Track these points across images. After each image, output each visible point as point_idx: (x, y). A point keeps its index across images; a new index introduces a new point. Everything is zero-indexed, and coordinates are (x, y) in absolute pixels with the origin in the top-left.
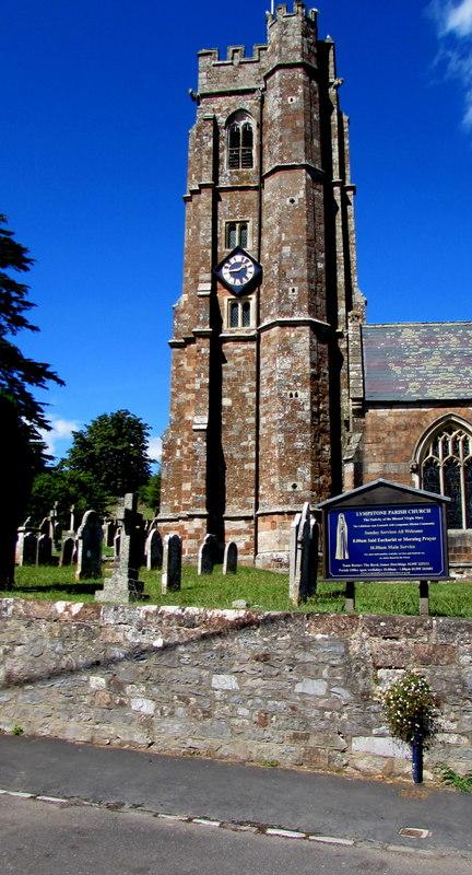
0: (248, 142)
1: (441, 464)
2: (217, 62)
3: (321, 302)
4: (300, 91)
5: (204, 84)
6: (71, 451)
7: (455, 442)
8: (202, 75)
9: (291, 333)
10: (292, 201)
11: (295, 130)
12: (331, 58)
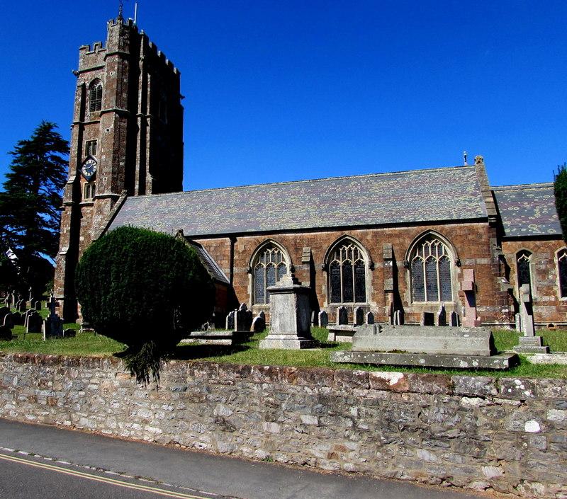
0: (100, 96)
1: (341, 264)
2: (88, 52)
4: (116, 68)
5: (81, 67)
7: (433, 246)
8: (81, 60)
9: (102, 202)
10: (108, 130)
11: (112, 91)
12: (142, 43)
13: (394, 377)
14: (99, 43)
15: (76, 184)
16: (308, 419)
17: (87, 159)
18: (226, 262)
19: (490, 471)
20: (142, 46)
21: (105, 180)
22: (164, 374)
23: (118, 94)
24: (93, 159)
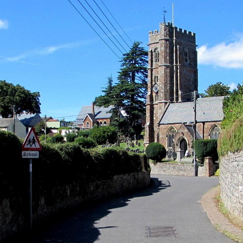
3: (168, 96)
4: (164, 46)
6: (212, 85)
9: (161, 105)
11: (163, 56)
13: (179, 164)
14: (157, 31)
15: (151, 96)
16: (172, 169)
17: (155, 84)
18: (202, 132)
19: (186, 173)
20: (174, 33)
21: (161, 95)
22: (158, 164)
23: (165, 58)
24: (157, 84)
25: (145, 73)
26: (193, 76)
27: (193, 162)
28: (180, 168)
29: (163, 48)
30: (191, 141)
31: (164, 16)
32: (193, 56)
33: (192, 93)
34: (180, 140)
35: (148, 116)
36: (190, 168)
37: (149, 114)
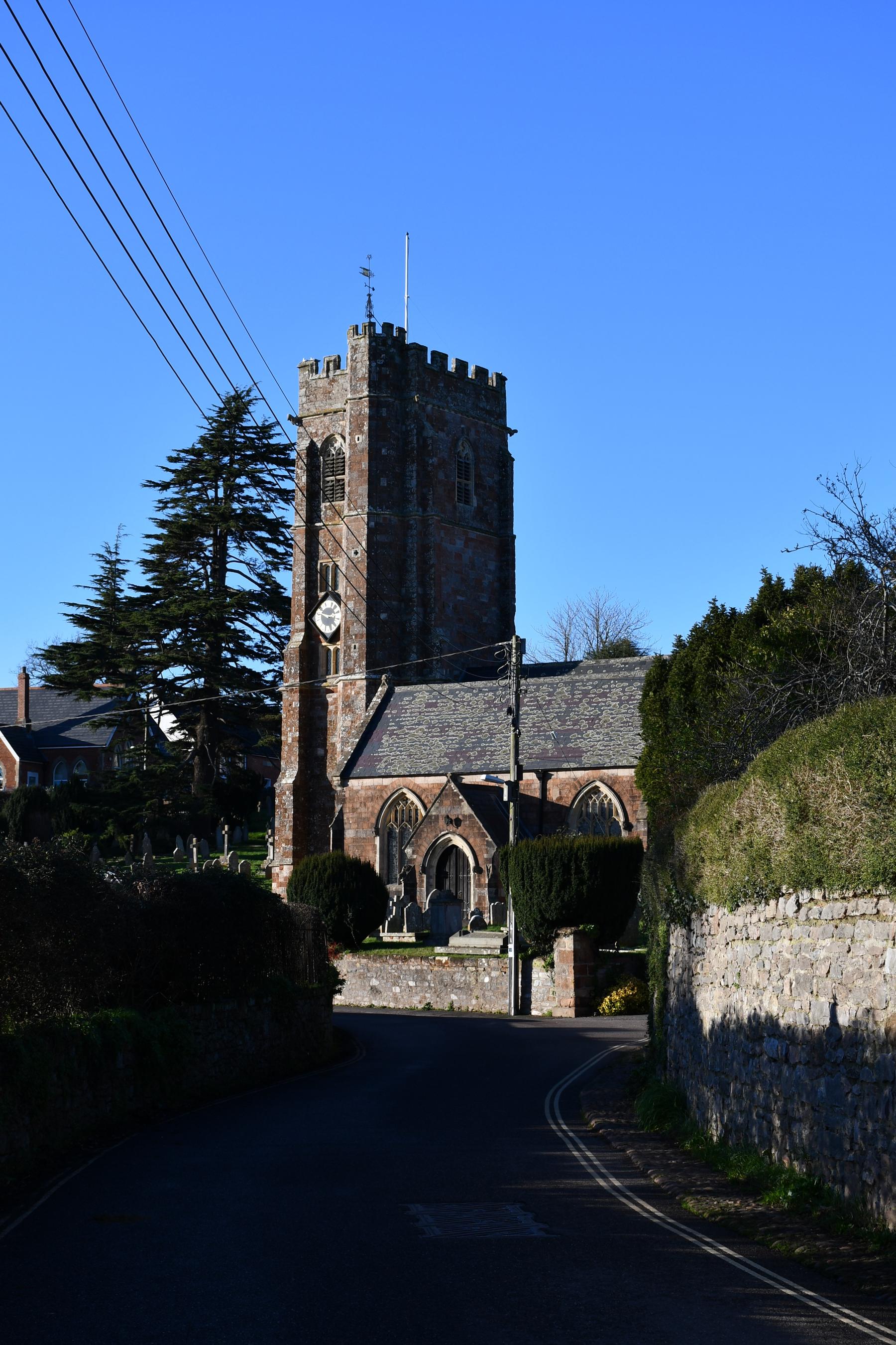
4: (366, 428)
16: (412, 984)
25: (270, 545)
26: (492, 566)
27: (504, 949)
28: (447, 979)
29: (362, 440)
30: (485, 856)
31: (369, 295)
32: (496, 477)
33: (502, 647)
34: (439, 852)
35: (290, 741)
36: (492, 979)
37: (297, 734)
